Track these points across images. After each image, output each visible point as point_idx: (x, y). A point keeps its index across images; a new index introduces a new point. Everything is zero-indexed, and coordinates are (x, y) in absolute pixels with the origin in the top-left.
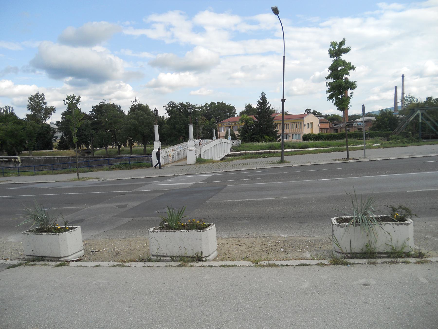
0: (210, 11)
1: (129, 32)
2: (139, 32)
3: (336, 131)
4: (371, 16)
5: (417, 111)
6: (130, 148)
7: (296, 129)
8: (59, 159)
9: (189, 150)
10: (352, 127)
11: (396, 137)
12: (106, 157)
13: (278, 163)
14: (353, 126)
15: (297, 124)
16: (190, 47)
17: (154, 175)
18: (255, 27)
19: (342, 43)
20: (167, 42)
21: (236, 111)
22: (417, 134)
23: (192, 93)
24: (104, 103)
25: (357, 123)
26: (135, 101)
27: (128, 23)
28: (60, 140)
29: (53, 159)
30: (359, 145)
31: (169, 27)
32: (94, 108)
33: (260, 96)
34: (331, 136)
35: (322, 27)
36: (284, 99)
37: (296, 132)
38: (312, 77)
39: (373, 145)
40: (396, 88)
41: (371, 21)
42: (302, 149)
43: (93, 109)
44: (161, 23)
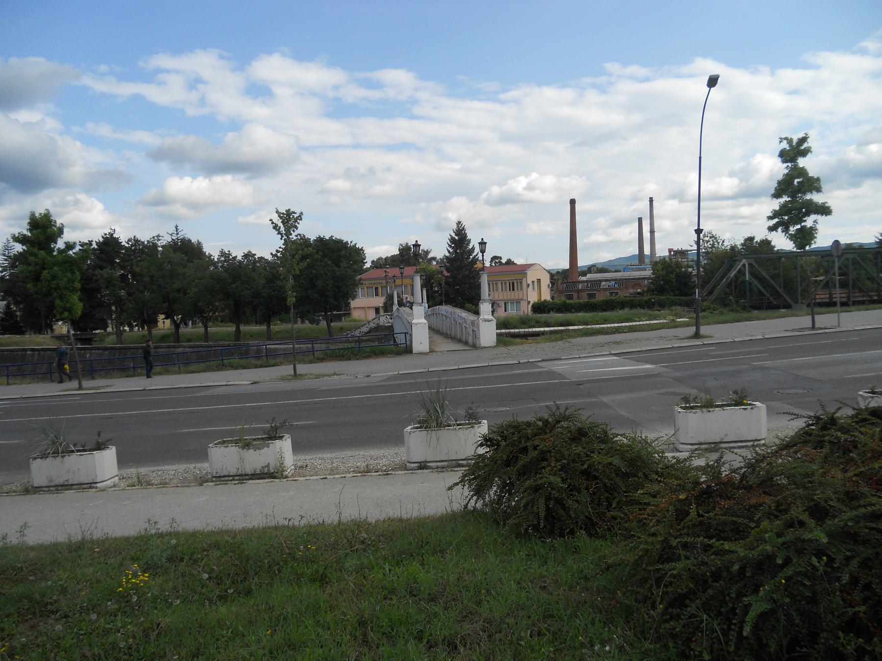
0: (284, 55)
1: (100, 87)
2: (128, 89)
3: (570, 297)
4: (594, 86)
5: (741, 260)
6: (202, 330)
7: (513, 293)
8: (36, 353)
9: (485, 321)
10: (599, 290)
11: (710, 306)
12: (159, 347)
13: (688, 338)
14: (601, 287)
15: (513, 283)
16: (237, 125)
17: (478, 363)
18: (375, 94)
19: (803, 140)
20: (191, 112)
21: (365, 257)
22: (743, 301)
23: (241, 219)
24: (112, 235)
25: (608, 283)
26: (175, 233)
27: (103, 68)
28: (3, 314)
29: (20, 353)
30: (655, 319)
31: (195, 82)
32: (82, 247)
33: (455, 227)
34: (587, 305)
35: (502, 102)
36: (701, 228)
37: (513, 298)
38: (485, 195)
39: (678, 320)
40: (640, 220)
41: (592, 96)
42: (562, 328)
43: (81, 248)
44: (177, 72)
